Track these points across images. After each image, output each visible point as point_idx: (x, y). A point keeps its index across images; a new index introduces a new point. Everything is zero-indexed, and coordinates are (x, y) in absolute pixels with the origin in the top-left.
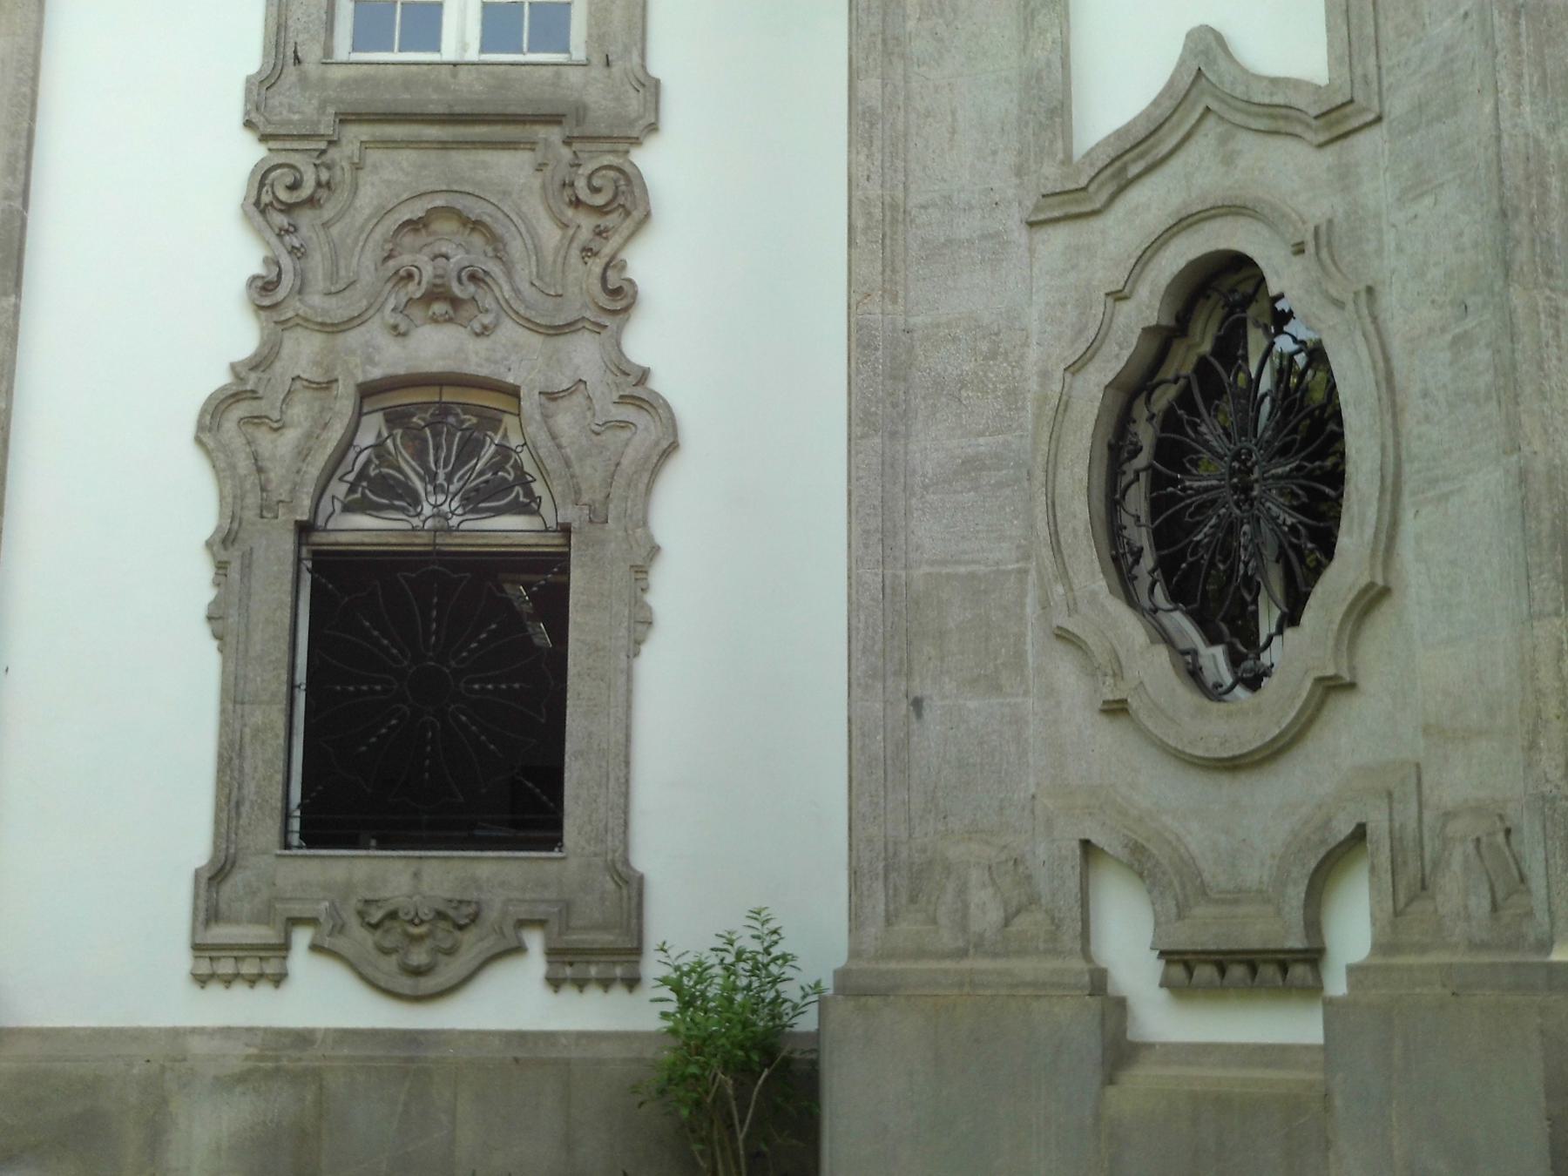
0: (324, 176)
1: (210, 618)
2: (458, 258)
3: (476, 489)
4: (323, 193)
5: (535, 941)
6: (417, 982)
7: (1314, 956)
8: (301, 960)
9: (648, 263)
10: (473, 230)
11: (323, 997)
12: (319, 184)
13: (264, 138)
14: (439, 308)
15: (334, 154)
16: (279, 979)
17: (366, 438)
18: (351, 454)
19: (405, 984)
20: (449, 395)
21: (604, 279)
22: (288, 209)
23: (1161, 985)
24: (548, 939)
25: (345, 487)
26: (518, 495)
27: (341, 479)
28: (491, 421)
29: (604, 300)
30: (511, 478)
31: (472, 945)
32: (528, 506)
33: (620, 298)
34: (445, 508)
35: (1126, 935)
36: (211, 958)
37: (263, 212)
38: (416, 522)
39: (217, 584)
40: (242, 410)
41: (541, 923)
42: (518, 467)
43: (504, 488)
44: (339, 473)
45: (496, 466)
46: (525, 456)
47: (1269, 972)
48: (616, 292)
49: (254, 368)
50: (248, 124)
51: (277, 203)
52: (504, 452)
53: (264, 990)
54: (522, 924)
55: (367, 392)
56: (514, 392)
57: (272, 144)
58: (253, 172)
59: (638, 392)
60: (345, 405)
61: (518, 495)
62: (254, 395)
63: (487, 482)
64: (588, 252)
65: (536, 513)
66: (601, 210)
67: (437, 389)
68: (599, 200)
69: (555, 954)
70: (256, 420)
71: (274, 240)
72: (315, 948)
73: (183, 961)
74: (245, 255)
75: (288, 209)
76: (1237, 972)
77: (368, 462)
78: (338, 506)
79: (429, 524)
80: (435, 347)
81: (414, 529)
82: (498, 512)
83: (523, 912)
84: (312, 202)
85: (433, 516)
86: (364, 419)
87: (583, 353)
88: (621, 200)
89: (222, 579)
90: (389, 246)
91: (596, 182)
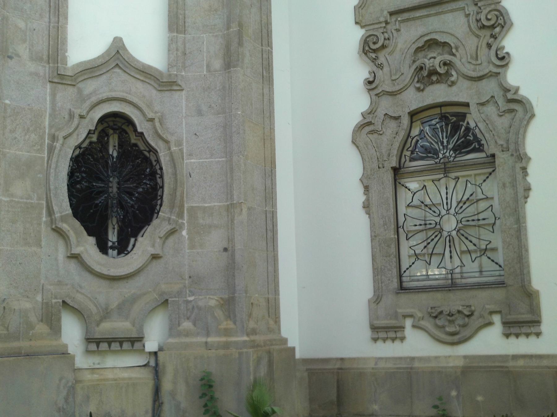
0: (386, 35)
1: (364, 207)
2: (439, 59)
3: (459, 146)
4: (387, 42)
5: (497, 319)
6: (456, 339)
7: (140, 339)
8: (409, 331)
9: (510, 43)
10: (443, 46)
11: (418, 345)
12: (385, 39)
13: (362, 27)
14: (434, 78)
15: (389, 27)
16: (402, 339)
17: (415, 132)
18: (410, 140)
19: (449, 339)
20: (444, 110)
21: (497, 54)
22: (374, 51)
23: (393, 342)
24: (502, 318)
25: (409, 153)
26: (475, 146)
27: (407, 150)
28: (463, 116)
29: (498, 63)
30: (472, 139)
31: (475, 322)
32: (480, 149)
33: (504, 60)
34: (447, 154)
35: (72, 333)
36: (395, 332)
37: (366, 54)
38: (437, 160)
39: (365, 194)
40: (368, 129)
41: (499, 312)
42: (475, 136)
43: (469, 143)
44: (406, 148)
45: (466, 135)
46: (477, 131)
47: (126, 346)
48: (503, 58)
49: (370, 113)
50: (357, 23)
51: (370, 49)
52: (468, 129)
53: (397, 343)
54: (491, 313)
55: (413, 115)
56: (467, 105)
57: (367, 28)
58: (361, 39)
59: (515, 97)
60: (406, 121)
61: (475, 146)
62: (370, 124)
63: (462, 142)
64: (489, 46)
65: (482, 151)
66: (493, 27)
67: (439, 109)
68: (492, 22)
69: (506, 324)
70: (372, 132)
71: (372, 64)
72: (414, 326)
73: (367, 333)
74: (361, 72)
75: (374, 51)
76: (126, 346)
77: (417, 141)
78: (408, 158)
79: (442, 161)
80: (438, 93)
81: (436, 163)
82: (468, 153)
83: (492, 307)
84: (383, 47)
85: (443, 158)
86: (414, 124)
87: (489, 87)
88: (500, 21)
89: (366, 192)
90: (413, 58)
91: (489, 17)
